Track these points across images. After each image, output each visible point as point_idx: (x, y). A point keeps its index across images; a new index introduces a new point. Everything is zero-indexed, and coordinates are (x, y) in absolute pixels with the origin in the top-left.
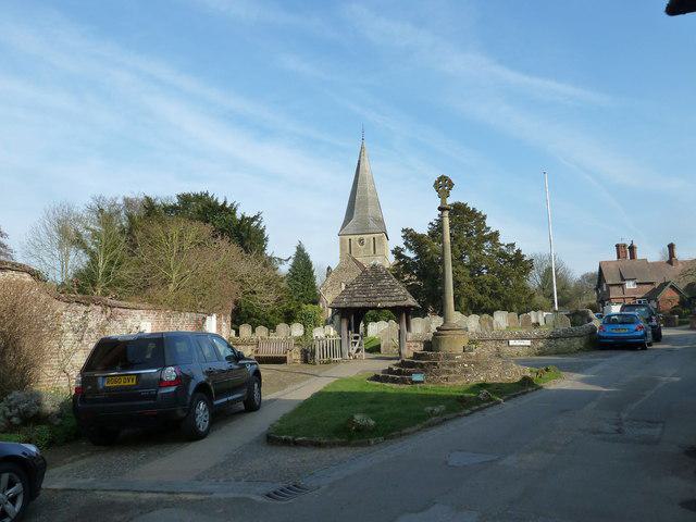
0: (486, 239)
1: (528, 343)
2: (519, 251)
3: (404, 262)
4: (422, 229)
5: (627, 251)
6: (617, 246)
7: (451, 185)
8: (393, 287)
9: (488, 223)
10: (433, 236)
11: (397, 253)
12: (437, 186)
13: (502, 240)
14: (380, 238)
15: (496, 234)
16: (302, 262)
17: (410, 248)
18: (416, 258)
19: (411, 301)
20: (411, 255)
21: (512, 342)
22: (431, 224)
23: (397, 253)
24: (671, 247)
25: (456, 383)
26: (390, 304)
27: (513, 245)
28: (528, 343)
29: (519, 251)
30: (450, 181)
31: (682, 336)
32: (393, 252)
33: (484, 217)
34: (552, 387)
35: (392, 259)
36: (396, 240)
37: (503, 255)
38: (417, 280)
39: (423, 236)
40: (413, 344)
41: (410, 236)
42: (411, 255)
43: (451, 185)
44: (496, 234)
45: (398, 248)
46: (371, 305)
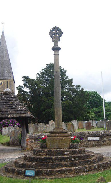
0: (66, 82)
1: (98, 138)
2: (82, 89)
3: (23, 94)
4: (33, 76)
7: (61, 33)
8: (18, 105)
9: (67, 74)
10: (39, 80)
11: (20, 89)
12: (51, 33)
13: (74, 83)
14: (10, 82)
15: (71, 80)
17: (27, 87)
18: (29, 92)
19: (29, 114)
20: (27, 90)
21: (89, 139)
22: (38, 74)
23: (20, 89)
25: (105, 161)
26: (15, 116)
27: (79, 86)
28: (98, 138)
29: (82, 89)
30: (60, 30)
31: (60, 155)
32: (17, 89)
33: (66, 71)
35: (16, 92)
36: (19, 82)
37: (74, 91)
38: (31, 103)
39: (33, 80)
40: (30, 141)
41: (26, 79)
42: (27, 90)
43: (61, 33)
44: (71, 80)
45: (20, 86)
46: (4, 116)
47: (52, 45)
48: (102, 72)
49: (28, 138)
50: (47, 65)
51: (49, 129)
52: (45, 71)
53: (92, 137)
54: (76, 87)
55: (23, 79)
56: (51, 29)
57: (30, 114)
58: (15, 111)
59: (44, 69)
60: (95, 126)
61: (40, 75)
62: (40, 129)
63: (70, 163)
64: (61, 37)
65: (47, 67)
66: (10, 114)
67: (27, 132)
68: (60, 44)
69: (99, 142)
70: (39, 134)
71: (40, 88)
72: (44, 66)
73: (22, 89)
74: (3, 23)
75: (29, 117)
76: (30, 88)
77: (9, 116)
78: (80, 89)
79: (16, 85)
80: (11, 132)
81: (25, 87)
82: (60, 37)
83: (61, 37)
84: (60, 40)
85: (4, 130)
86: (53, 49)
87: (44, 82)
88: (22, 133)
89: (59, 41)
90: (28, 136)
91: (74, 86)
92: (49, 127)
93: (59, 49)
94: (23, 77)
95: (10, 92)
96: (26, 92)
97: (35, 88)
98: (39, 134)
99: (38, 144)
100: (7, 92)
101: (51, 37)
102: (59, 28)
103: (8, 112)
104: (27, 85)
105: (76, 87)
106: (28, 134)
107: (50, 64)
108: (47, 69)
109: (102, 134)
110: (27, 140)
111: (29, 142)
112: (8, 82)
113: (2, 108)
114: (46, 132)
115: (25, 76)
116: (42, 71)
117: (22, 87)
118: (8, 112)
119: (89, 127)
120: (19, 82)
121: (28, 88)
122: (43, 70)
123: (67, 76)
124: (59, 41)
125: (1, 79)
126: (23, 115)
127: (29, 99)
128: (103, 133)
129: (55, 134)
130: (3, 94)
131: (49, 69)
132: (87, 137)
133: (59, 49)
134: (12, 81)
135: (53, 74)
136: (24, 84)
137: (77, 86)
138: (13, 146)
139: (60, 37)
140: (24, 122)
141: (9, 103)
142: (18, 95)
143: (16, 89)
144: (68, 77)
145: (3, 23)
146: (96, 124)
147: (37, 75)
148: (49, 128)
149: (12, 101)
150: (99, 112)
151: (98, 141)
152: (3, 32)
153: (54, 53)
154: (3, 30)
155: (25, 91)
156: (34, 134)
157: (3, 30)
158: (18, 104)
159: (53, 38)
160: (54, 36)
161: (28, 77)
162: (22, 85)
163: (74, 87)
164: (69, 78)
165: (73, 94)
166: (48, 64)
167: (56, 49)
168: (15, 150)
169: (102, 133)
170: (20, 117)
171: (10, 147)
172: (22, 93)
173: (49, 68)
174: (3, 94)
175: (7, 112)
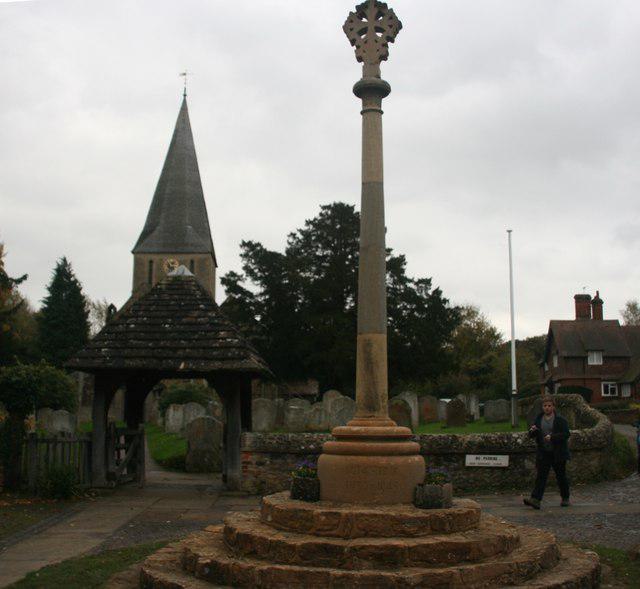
1: (503, 461)
4: (278, 244)
5: (588, 305)
6: (430, 280)
11: (231, 281)
15: (401, 260)
16: (64, 285)
17: (255, 278)
18: (261, 294)
19: (254, 362)
20: (253, 287)
21: (470, 460)
24: (25, 277)
27: (427, 282)
28: (503, 461)
29: (438, 292)
30: (392, 16)
32: (224, 281)
34: (637, 455)
37: (409, 295)
39: (275, 256)
40: (254, 458)
41: (254, 252)
42: (253, 287)
44: (401, 260)
45: (233, 274)
47: (356, 72)
48: (509, 231)
49: (247, 449)
50: (324, 208)
51: (323, 419)
52: (315, 225)
53: (482, 457)
54: (416, 284)
55: (243, 251)
56: (354, 11)
57: (259, 362)
58: (204, 348)
59: (312, 219)
60: (477, 417)
61: (300, 241)
62: (291, 416)
63: (424, 576)
64: (393, 41)
65: (321, 214)
66: (186, 358)
67: (247, 425)
68: (387, 71)
69: (508, 472)
70: (290, 435)
71: (298, 282)
72: (314, 213)
73: (239, 283)
74: (185, 74)
75: (254, 374)
76: (265, 281)
77: (182, 366)
78: (430, 292)
79: (221, 272)
80: (190, 425)
81: (249, 279)
82: (389, 44)
83: (393, 41)
84: (387, 54)
85: (171, 416)
86: (360, 90)
87: (311, 263)
88: (226, 428)
89: (385, 57)
90: (248, 443)
91: (411, 281)
92: (323, 412)
93: (384, 90)
94: (244, 244)
95: (188, 280)
96: (251, 295)
97: (280, 283)
98: (290, 435)
99: (284, 471)
100: (177, 279)
101: (353, 42)
102: (385, 5)
103: (180, 352)
104: (256, 271)
105: (416, 284)
106: (248, 435)
107: (332, 204)
108: (322, 221)
109: (518, 444)
110: (243, 455)
111: (249, 463)
112: (196, 264)
113: (157, 336)
114: (313, 431)
115: (250, 243)
116: (305, 228)
117: (240, 278)
118: (180, 352)
119: (458, 416)
120: (229, 260)
121: (256, 282)
122: (308, 223)
123: (388, 246)
124: (386, 59)
125: (174, 251)
126: (236, 365)
127: (258, 318)
128: (524, 442)
129: (365, 458)
130: (163, 287)
131: (328, 222)
132: (463, 456)
133: (384, 90)
134: (205, 259)
135: (346, 235)
136: (246, 268)
137: (421, 281)
138: (196, 472)
139: (389, 44)
140: (235, 390)
141: (184, 320)
142: (224, 304)
143: (218, 281)
144: (389, 250)
145: (185, 74)
146: (482, 410)
147: (291, 240)
148: (323, 416)
149: (196, 313)
150: (483, 371)
151: (504, 468)
152: (185, 102)
153: (364, 104)
154: (185, 95)
155: (248, 292)
156: (271, 435)
157: (185, 95)
158: (217, 324)
159: (358, 47)
160: (363, 37)
161: (259, 244)
162: (240, 272)
163: (411, 285)
164: (395, 254)
165: (405, 308)
166: (328, 204)
167: (372, 92)
168: (201, 489)
169: (519, 440)
170: (222, 372)
171: (183, 476)
172: (237, 297)
173: (329, 217)
174: (163, 287)
175: (175, 349)
